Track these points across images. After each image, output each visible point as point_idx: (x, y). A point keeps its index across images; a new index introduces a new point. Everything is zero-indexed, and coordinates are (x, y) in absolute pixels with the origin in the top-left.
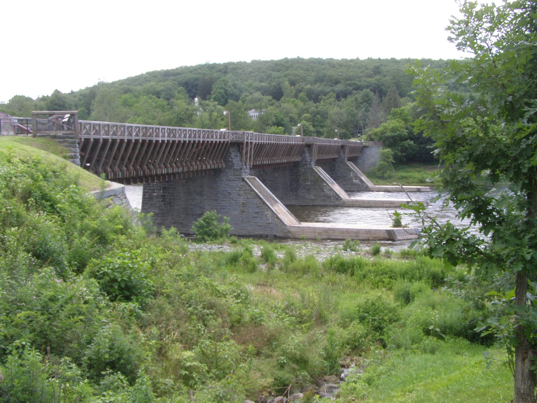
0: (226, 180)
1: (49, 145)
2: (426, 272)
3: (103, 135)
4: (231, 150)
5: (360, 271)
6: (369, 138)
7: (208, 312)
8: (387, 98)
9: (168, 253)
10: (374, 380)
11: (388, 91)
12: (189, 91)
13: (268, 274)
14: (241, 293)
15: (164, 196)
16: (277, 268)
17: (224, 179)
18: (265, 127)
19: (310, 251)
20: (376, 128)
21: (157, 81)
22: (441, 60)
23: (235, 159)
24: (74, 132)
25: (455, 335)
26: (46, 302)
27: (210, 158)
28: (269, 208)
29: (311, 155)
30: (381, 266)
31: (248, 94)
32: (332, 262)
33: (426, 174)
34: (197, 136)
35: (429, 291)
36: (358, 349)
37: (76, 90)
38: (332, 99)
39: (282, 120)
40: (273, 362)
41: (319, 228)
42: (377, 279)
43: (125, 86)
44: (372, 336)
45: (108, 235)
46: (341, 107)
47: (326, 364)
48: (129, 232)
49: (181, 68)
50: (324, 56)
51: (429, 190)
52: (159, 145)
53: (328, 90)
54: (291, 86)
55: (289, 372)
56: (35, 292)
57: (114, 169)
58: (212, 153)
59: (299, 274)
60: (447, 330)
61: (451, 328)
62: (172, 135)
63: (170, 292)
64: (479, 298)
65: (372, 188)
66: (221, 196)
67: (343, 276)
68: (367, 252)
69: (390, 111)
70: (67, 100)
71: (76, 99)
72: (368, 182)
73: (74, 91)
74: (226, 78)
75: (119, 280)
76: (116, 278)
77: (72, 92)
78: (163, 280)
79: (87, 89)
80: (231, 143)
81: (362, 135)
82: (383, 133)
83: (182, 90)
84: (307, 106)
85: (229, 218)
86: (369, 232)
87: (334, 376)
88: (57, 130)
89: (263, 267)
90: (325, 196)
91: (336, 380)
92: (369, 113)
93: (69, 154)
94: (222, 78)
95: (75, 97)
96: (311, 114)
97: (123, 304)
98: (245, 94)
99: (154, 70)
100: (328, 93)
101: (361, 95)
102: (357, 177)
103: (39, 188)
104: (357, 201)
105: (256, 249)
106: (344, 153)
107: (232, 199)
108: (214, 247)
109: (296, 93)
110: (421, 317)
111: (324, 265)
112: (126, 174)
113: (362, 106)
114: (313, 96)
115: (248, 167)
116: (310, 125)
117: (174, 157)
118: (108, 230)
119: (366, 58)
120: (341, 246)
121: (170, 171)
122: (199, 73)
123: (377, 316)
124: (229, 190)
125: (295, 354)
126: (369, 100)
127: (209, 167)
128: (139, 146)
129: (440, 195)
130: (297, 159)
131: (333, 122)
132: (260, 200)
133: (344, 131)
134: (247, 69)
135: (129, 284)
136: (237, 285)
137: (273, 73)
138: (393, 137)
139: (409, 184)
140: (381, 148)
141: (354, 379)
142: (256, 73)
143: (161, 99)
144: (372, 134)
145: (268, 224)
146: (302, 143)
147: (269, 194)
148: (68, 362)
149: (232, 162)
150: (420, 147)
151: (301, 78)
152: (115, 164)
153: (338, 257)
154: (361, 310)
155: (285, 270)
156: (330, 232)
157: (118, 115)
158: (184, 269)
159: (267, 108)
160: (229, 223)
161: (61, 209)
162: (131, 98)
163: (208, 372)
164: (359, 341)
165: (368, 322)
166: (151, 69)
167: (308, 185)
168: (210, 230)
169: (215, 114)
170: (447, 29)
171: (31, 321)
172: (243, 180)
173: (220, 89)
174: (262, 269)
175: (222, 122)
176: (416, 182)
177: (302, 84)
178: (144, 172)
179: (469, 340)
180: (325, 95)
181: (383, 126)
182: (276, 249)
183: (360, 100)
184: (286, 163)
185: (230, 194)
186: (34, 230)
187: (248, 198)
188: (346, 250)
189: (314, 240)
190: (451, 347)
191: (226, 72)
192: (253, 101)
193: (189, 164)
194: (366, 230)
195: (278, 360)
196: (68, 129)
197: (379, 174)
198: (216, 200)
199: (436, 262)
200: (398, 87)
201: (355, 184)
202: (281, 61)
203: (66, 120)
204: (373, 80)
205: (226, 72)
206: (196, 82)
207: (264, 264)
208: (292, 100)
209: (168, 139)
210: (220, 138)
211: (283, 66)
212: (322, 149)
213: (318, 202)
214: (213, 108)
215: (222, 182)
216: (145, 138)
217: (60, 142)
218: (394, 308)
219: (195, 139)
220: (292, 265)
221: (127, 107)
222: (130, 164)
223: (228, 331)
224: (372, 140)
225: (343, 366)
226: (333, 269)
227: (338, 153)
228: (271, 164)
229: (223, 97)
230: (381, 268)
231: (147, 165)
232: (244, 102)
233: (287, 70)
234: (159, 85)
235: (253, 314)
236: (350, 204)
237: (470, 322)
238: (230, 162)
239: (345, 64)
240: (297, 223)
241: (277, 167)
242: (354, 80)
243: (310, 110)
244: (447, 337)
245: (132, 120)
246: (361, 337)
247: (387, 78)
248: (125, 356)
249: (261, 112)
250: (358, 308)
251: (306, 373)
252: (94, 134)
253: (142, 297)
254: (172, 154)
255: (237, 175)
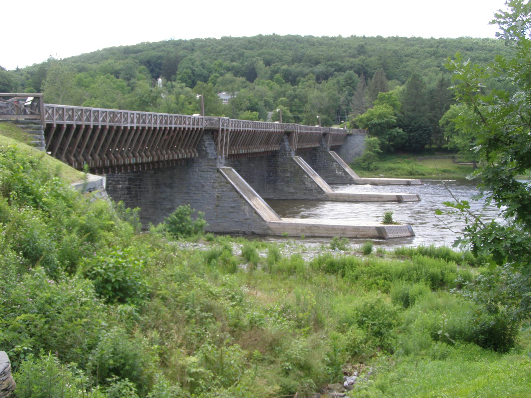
0: (199, 170)
1: (10, 131)
2: (423, 274)
3: (67, 120)
4: (205, 137)
5: (351, 271)
6: (352, 125)
7: (206, 315)
8: (373, 81)
9: (158, 251)
10: (387, 387)
11: (373, 73)
12: (152, 71)
13: (251, 275)
14: (236, 294)
15: (130, 188)
16: (259, 268)
17: (197, 169)
18: (238, 112)
19: (294, 250)
20: (361, 113)
21: (116, 59)
22: (432, 38)
23: (210, 148)
24: (38, 117)
25: (465, 340)
26: (43, 304)
27: (182, 146)
28: (247, 202)
29: (291, 144)
30: (374, 266)
31: (218, 75)
32: (320, 262)
33: (416, 165)
34: (169, 122)
35: (430, 294)
36: (358, 356)
37: (22, 66)
38: (312, 82)
39: (257, 104)
40: (277, 368)
41: (302, 224)
42: (371, 280)
43: (79, 63)
44: (373, 342)
45: (98, 231)
46: (322, 91)
47: (331, 370)
48: (115, 229)
49: (143, 44)
50: (303, 33)
51: (420, 183)
52: (127, 133)
53: (307, 71)
54: (266, 66)
55: (295, 379)
56: (29, 293)
57: (78, 158)
58: (184, 140)
59: (285, 275)
60: (457, 335)
61: (461, 333)
62: (141, 121)
63: (165, 294)
64: (492, 301)
65: (358, 181)
66: (193, 189)
67: (333, 278)
68: (358, 252)
69: (377, 95)
70: (12, 79)
71: (23, 77)
72: (352, 174)
73: (20, 68)
74: (193, 57)
75: (113, 280)
76: (109, 279)
77: (18, 69)
78: (156, 280)
79: (35, 66)
80: (205, 130)
81: (345, 121)
82: (369, 119)
83: (144, 69)
84: (283, 89)
85: (204, 213)
86: (356, 229)
87: (338, 384)
88: (18, 114)
89: (244, 267)
90: (306, 189)
91: (341, 388)
92: (353, 97)
93: (34, 142)
94: (189, 57)
95: (22, 75)
96: (288, 98)
97: (120, 307)
98: (215, 74)
99: (112, 46)
100: (307, 74)
101: (343, 77)
102: (340, 168)
103: (20, 180)
104: (341, 195)
105: (235, 248)
106: (327, 142)
107: (206, 191)
108: (188, 245)
109: (271, 74)
110: (428, 321)
111: (311, 265)
112: (100, 163)
113: (345, 89)
114: (290, 77)
115: (224, 156)
116: (287, 109)
117: (143, 146)
118: (97, 226)
119: (350, 36)
120: (329, 245)
121: (139, 160)
122: (163, 51)
123: (377, 320)
124: (202, 181)
125: (300, 360)
126: (352, 83)
127: (181, 157)
128: (106, 133)
129: (482, 193)
130: (276, 148)
131: (313, 107)
132: (236, 194)
133: (325, 117)
134: (217, 47)
135: (124, 285)
136: (230, 286)
137: (245, 51)
138: (379, 125)
139: (397, 176)
140: (367, 136)
141: (365, 386)
142: (227, 51)
143: (120, 80)
144: (357, 121)
145: (245, 219)
146: (281, 130)
147: (247, 187)
148: (75, 368)
149: (205, 151)
150: (409, 136)
151: (277, 58)
152: (79, 153)
153: (328, 257)
154: (360, 314)
155: (269, 270)
156: (315, 228)
157: (72, 97)
158: (177, 269)
159: (239, 90)
160: (204, 218)
161: (45, 203)
162: (86, 78)
163: (214, 378)
164: (358, 347)
165: (368, 327)
166: (109, 45)
167: (288, 177)
168: (183, 226)
169: (182, 96)
170: (490, 23)
171: (28, 325)
172: (218, 171)
173: (187, 69)
174: (243, 269)
175: (190, 106)
176: (405, 175)
177: (279, 65)
178: (111, 162)
179: (480, 346)
180: (304, 77)
181: (369, 112)
182: (257, 247)
183: (342, 82)
184: (264, 152)
185: (203, 186)
186: (21, 227)
187: (223, 191)
188: (334, 249)
189: (297, 237)
190: (462, 353)
191: (193, 50)
192: (224, 83)
193: (159, 153)
194: (353, 227)
195: (282, 367)
196: (32, 113)
197: (364, 165)
198: (188, 193)
199: (435, 263)
200: (385, 67)
201: (338, 176)
202: (254, 38)
203: (30, 103)
204: (356, 61)
205: (193, 50)
206: (159, 61)
207: (245, 263)
208: (267, 82)
209: (138, 125)
210: (193, 124)
211: (257, 43)
212: (302, 137)
213: (298, 196)
214: (180, 90)
215: (194, 173)
216: (112, 124)
217: (23, 128)
218: (395, 312)
219: (166, 126)
220: (276, 265)
221: (83, 88)
222: (96, 152)
223: (228, 335)
224: (356, 127)
225: (346, 374)
226: (322, 270)
227: (320, 142)
228: (247, 154)
229: (190, 77)
230: (375, 268)
231: (113, 154)
232: (214, 84)
233: (261, 49)
234: (117, 64)
235: (253, 318)
236: (334, 198)
237: (481, 326)
238: (204, 151)
239: (325, 42)
240: (277, 219)
241: (252, 157)
242: (336, 59)
243: (287, 93)
244: (457, 343)
245: (89, 103)
246: (361, 343)
247: (373, 59)
248: (130, 362)
249: (234, 95)
250: (356, 312)
251: (312, 381)
252: (57, 120)
253: (139, 300)
254: (142, 141)
255: (211, 166)
